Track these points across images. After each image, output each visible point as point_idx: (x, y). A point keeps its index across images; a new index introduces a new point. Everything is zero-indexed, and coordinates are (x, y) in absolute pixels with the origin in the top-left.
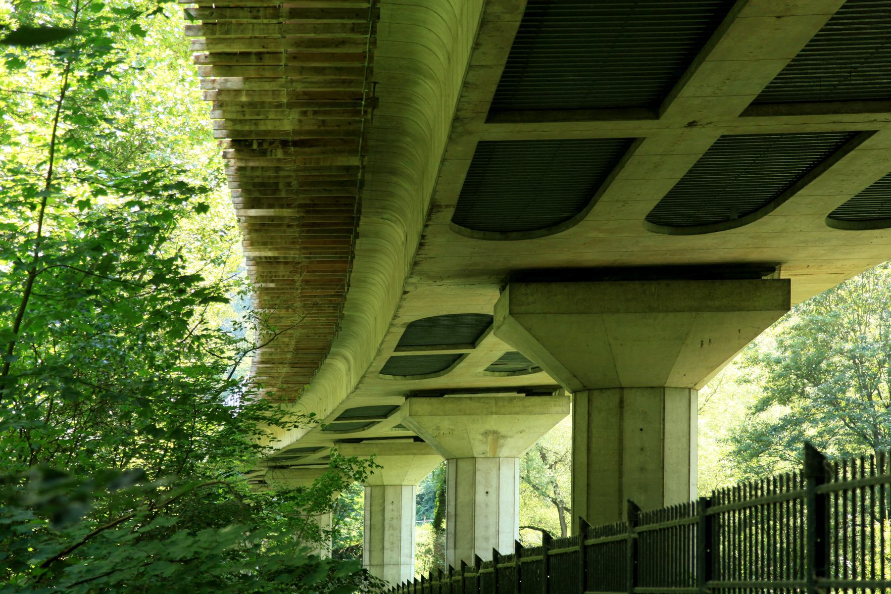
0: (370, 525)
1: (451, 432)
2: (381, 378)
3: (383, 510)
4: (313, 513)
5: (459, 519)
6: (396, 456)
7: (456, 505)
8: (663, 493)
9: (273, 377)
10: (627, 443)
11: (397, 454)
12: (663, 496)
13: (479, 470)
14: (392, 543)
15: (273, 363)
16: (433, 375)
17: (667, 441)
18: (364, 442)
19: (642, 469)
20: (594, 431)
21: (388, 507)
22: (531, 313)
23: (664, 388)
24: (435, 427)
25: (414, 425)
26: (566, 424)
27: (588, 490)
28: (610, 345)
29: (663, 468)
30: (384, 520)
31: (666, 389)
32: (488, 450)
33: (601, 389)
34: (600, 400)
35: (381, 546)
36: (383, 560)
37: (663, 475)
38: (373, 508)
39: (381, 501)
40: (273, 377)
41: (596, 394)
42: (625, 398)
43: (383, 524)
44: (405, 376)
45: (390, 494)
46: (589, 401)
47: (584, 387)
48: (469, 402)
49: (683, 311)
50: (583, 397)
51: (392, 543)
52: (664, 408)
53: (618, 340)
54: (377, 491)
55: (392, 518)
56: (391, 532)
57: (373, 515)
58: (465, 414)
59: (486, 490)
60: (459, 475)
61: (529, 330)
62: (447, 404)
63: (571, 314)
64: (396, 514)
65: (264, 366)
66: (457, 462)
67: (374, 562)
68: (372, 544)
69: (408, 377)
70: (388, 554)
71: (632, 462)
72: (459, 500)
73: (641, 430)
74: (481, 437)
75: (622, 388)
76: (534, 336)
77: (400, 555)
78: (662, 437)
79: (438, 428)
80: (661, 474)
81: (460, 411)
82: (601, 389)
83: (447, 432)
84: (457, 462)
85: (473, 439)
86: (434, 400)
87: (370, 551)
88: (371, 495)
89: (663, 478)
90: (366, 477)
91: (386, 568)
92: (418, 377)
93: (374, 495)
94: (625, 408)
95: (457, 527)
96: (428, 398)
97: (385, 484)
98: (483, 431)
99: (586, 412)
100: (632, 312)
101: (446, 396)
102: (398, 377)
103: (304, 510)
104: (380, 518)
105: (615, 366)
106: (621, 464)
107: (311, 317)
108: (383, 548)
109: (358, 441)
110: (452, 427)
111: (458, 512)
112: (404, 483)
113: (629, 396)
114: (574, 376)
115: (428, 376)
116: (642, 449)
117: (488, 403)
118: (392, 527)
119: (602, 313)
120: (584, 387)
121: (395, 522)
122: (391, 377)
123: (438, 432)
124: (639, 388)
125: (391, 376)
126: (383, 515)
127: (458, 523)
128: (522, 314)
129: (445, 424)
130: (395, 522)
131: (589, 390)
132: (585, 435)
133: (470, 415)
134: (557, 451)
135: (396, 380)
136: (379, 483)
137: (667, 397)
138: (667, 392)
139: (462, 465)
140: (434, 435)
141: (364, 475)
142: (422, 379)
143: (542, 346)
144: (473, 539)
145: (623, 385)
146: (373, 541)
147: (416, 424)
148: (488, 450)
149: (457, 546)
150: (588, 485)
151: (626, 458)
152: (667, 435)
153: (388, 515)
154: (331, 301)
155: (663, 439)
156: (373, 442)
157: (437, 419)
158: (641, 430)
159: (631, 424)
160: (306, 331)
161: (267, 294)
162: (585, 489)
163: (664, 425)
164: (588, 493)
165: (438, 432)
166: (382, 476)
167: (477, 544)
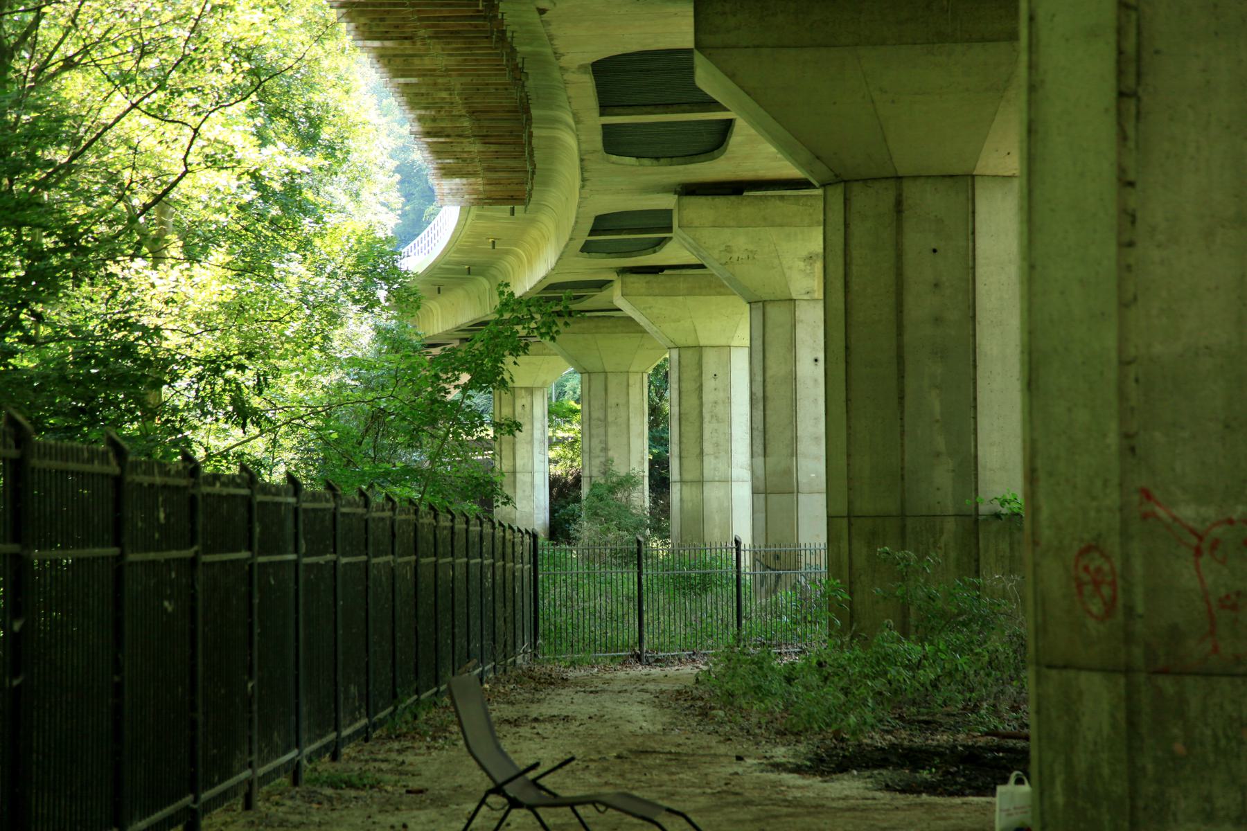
0: (680, 414)
1: (751, 256)
2: (613, 163)
3: (700, 388)
4: (470, 392)
5: (770, 405)
6: (719, 297)
7: (764, 381)
8: (975, 361)
9: (464, 160)
10: (909, 272)
11: (720, 294)
12: (975, 367)
13: (802, 321)
14: (717, 445)
15: (448, 136)
16: (702, 156)
17: (980, 271)
18: (666, 272)
19: (938, 320)
20: (856, 253)
21: (709, 384)
22: (734, 47)
23: (973, 177)
24: (723, 248)
25: (689, 244)
26: (815, 241)
27: (847, 356)
28: (873, 102)
29: (974, 317)
30: (701, 405)
31: (976, 178)
32: (816, 288)
33: (865, 180)
34: (863, 199)
35: (698, 451)
36: (702, 474)
37: (974, 330)
38: (683, 385)
39: (696, 373)
40: (464, 160)
41: (856, 188)
42: (904, 195)
43: (701, 412)
44: (657, 158)
45: (710, 360)
46: (846, 201)
47: (836, 176)
48: (778, 203)
49: (998, 40)
50: (837, 194)
51: (717, 445)
52: (974, 212)
53: (886, 92)
54: (689, 356)
55: (716, 403)
56: (715, 425)
57: (684, 398)
58: (773, 225)
59: (815, 356)
60: (768, 330)
61: (732, 76)
62: (745, 206)
63: (802, 47)
64: (721, 395)
65: (435, 140)
66: (764, 307)
67: (687, 477)
68: (683, 446)
69: (662, 161)
70: (709, 462)
71: (919, 306)
72: (769, 373)
73: (935, 251)
74: (802, 265)
75: (899, 178)
76: (742, 87)
77: (730, 465)
78: (971, 263)
79: (728, 249)
80: (971, 327)
81: (765, 219)
82: (865, 180)
83: (745, 256)
84: (764, 307)
85: (790, 268)
86: (720, 201)
87: (681, 458)
88: (679, 362)
89: (974, 336)
90: (557, 332)
91: (707, 487)
92: (680, 160)
93: (683, 363)
94: (906, 214)
95: (768, 420)
96: (710, 198)
97: (702, 344)
98: (805, 253)
99: (842, 220)
100: (907, 43)
101: (745, 194)
102: (645, 161)
103: (456, 387)
104: (695, 402)
105: (885, 140)
106: (901, 312)
107: (461, 55)
108: (702, 452)
109: (656, 270)
110: (751, 247)
111: (768, 394)
112: (733, 344)
113: (912, 192)
114: (818, 158)
115: (696, 158)
116: (936, 285)
117: (811, 206)
118: (714, 416)
119: (857, 45)
120: (836, 176)
121: (720, 409)
122: (632, 160)
123: (729, 256)
124: (929, 177)
125: (634, 159)
126: (701, 398)
127: (768, 412)
128: (718, 48)
129: (741, 241)
130: (720, 409)
131: (845, 182)
132: (841, 261)
133: (781, 225)
134: (808, 290)
135: (641, 165)
136: (691, 342)
137: (977, 192)
138: (978, 185)
139: (772, 311)
140: (723, 261)
141: (554, 329)
142: (686, 164)
143: (757, 106)
144: (795, 439)
145: (900, 174)
146: (684, 440)
147: (691, 241)
148: (816, 288)
149: (768, 451)
150: (847, 348)
151: (909, 301)
152: (980, 260)
153: (708, 397)
154: (476, 26)
155: (974, 268)
156: (684, 272)
157: (726, 234)
158: (935, 251)
159: (916, 241)
160: (468, 79)
161: (362, 13)
162: (843, 354)
163: (974, 241)
164: (847, 362)
165: (729, 256)
166: (695, 330)
167: (801, 448)
